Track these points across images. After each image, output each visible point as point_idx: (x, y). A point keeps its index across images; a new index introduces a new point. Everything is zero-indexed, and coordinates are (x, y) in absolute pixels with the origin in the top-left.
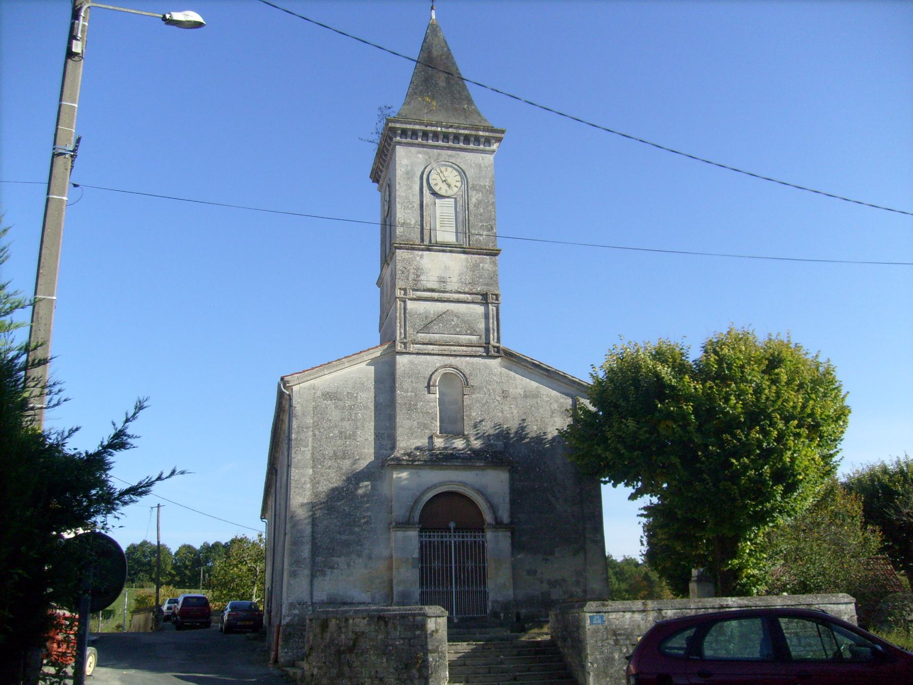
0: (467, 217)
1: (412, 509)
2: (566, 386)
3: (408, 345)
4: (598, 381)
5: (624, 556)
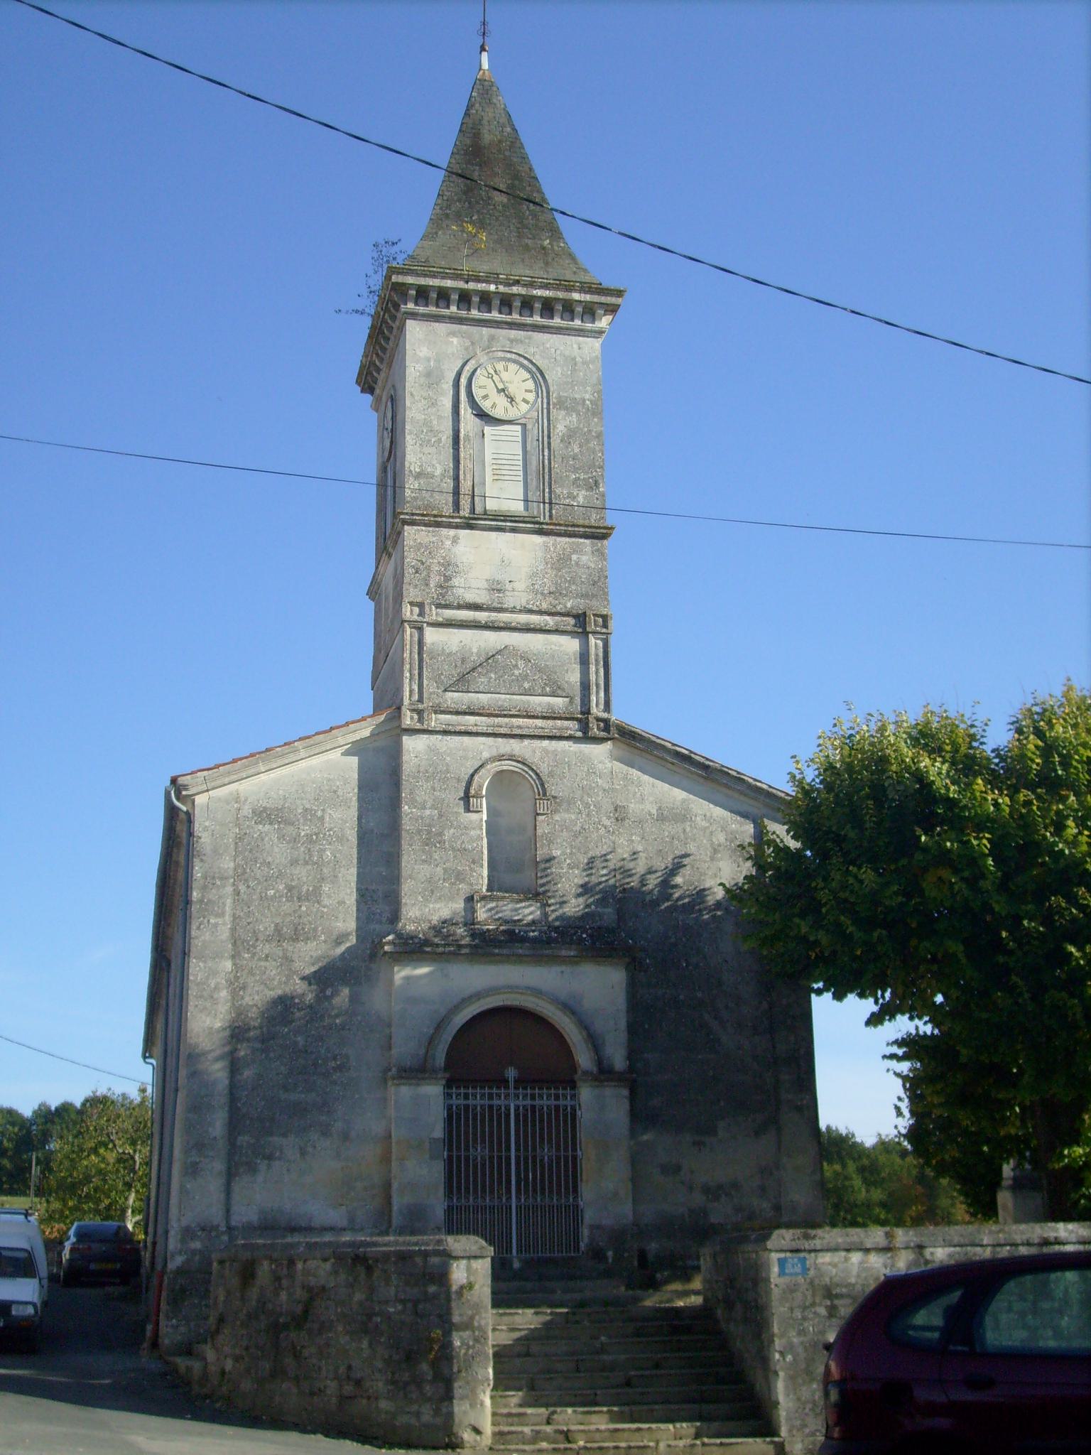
0: (546, 462)
1: (431, 1041)
2: (742, 798)
3: (425, 715)
4: (803, 788)
5: (879, 1135)
